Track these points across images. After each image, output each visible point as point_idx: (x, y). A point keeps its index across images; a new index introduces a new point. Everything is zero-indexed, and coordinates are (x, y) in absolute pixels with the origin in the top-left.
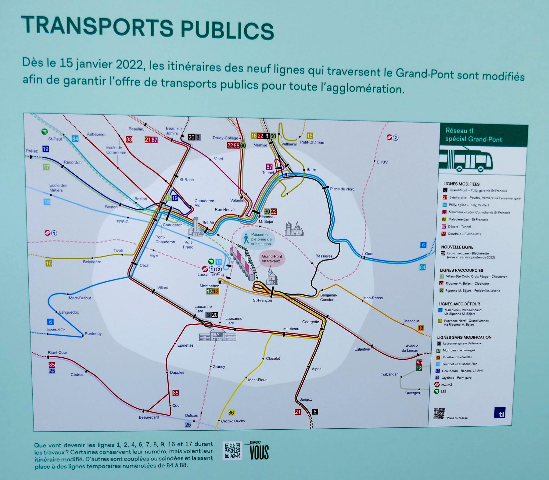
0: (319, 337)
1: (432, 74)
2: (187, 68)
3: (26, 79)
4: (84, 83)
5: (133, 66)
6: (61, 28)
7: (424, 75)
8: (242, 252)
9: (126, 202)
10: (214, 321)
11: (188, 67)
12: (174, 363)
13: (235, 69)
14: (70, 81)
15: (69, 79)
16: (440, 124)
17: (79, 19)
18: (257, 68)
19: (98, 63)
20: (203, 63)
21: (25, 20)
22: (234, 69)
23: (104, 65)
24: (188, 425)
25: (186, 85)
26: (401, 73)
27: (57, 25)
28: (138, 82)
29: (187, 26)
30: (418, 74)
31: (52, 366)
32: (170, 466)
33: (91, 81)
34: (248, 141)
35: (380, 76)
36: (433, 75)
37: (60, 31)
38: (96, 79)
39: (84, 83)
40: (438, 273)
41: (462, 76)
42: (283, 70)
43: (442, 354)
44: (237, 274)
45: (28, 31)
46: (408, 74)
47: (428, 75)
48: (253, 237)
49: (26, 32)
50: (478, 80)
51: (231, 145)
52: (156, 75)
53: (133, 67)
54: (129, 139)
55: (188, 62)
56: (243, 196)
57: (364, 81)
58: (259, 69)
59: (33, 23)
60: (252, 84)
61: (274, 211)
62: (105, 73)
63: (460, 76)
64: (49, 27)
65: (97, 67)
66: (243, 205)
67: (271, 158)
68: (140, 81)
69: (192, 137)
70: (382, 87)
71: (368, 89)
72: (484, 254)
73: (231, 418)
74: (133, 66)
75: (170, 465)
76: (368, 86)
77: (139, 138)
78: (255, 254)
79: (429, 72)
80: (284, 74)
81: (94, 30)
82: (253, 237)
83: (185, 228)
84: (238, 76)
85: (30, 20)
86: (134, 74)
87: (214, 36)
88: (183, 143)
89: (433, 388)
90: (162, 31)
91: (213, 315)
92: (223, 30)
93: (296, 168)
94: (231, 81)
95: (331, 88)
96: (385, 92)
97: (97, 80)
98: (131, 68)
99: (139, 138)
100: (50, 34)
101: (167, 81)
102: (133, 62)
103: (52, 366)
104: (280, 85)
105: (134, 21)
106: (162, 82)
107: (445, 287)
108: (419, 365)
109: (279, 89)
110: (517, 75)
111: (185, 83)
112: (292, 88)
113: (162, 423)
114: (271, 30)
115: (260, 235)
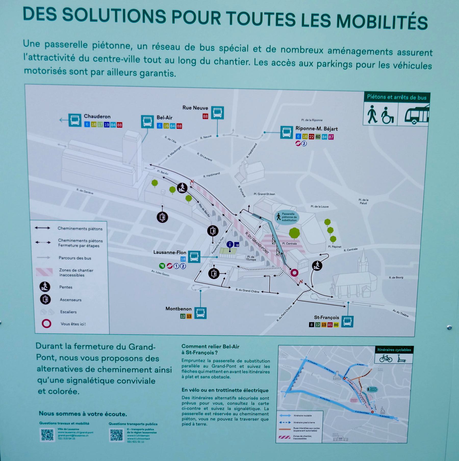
2: (273, 51)
3: (30, 57)
4: (46, 59)
6: (168, 118)
13: (256, 49)
16: (364, 92)
17: (152, 11)
20: (99, 42)
21: (229, 15)
29: (177, 14)
33: (232, 62)
37: (168, 119)
38: (236, 60)
39: (30, 59)
41: (73, 72)
48: (283, 215)
49: (23, 19)
50: (432, 56)
58: (313, 50)
60: (280, 62)
70: (32, 55)
72: (291, 214)
80: (359, 55)
81: (71, 18)
82: (283, 215)
85: (271, 16)
87: (369, 27)
90: (48, 16)
92: (376, 22)
96: (237, 65)
97: (146, 59)
101: (113, 58)
104: (371, 64)
105: (369, 17)
106: (144, 59)
109: (369, 67)
110: (158, 44)
114: (426, 22)
115: (288, 214)
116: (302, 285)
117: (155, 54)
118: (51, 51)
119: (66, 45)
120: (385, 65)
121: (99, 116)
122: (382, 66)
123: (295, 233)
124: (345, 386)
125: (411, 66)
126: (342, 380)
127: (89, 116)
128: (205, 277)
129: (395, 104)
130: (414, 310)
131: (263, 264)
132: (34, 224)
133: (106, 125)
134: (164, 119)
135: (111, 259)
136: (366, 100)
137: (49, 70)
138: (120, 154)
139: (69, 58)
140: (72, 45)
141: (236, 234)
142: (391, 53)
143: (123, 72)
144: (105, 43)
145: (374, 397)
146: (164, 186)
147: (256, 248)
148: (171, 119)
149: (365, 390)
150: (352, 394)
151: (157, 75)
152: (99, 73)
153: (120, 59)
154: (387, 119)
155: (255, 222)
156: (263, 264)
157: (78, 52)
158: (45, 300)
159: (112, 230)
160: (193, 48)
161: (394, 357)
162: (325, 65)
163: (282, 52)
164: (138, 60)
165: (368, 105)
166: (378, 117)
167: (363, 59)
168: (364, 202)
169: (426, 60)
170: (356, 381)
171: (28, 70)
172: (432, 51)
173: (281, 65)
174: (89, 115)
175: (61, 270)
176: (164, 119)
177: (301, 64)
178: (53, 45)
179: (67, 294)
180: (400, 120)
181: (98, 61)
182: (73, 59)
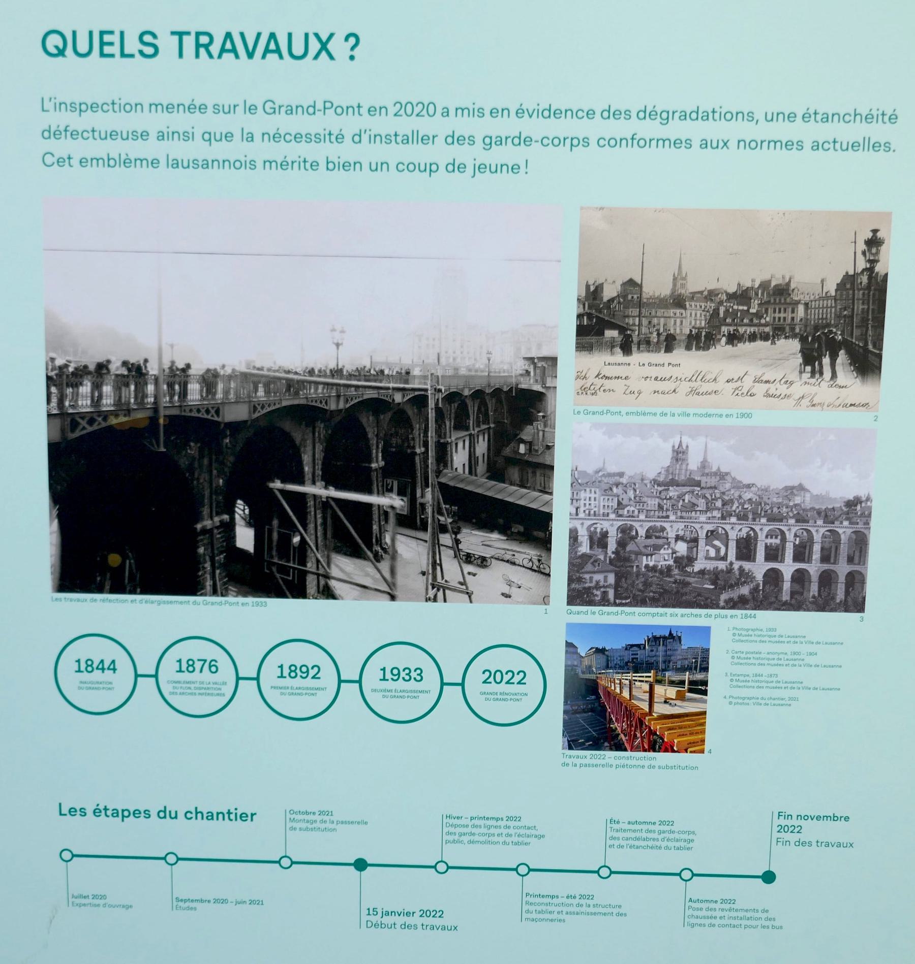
1: (325, 108)
5: (398, 112)
7: (311, 110)
14: (494, 140)
15: (491, 138)
18: (618, 113)
19: (534, 110)
21: (176, 38)
22: (616, 115)
25: (318, 140)
26: (271, 108)
27: (229, 46)
28: (529, 139)
30: (836, 117)
32: (97, 668)
35: (361, 115)
36: (326, 110)
37: (276, 56)
42: (664, 115)
45: (181, 55)
46: (283, 109)
47: (320, 110)
53: (398, 114)
55: (519, 105)
59: (189, 42)
60: (605, 140)
64: (215, 49)
65: (533, 116)
68: (149, 132)
74: (398, 112)
75: (95, 666)
76: (276, 132)
79: (320, 106)
85: (185, 38)
95: (818, 146)
98: (417, 115)
100: (216, 61)
102: (420, 106)
111: (186, 134)
112: (332, 140)
120: (302, 137)
127: (197, 813)
137: (295, 161)
139: (332, 136)
142: (628, 115)
143: (87, 160)
144: (812, 111)
151: (208, 167)
153: (531, 140)
163: (456, 116)
169: (878, 132)
171: (141, 161)
172: (361, 105)
173: (551, 145)
177: (704, 144)
181: (293, 140)
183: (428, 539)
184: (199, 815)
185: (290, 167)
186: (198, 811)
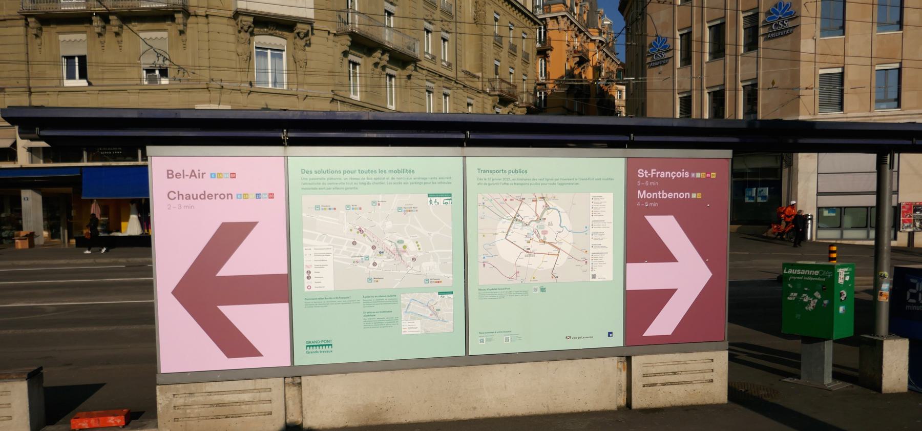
0: (558, 255)
6: (195, 176)
8: (536, 231)
9: (505, 217)
10: (529, 251)
11: (522, 180)
12: (518, 264)
23: (499, 180)
24: (522, 282)
31: (484, 265)
34: (538, 199)
37: (194, 177)
40: (591, 222)
43: (593, 259)
44: (535, 237)
47: (186, 176)
51: (533, 201)
52: (513, 182)
54: (506, 200)
56: (537, 215)
57: (569, 182)
61: (545, 219)
62: (500, 182)
63: (596, 180)
66: (537, 217)
67: (544, 204)
69: (523, 199)
71: (570, 184)
73: (534, 279)
77: (508, 199)
78: (540, 232)
83: (521, 224)
84: (535, 182)
86: (507, 182)
88: (520, 201)
89: (591, 269)
91: (529, 249)
93: (551, 207)
94: (533, 183)
99: (508, 199)
103: (484, 265)
107: (593, 226)
108: (586, 262)
113: (514, 282)
116: (409, 267)
117: (351, 181)
118: (311, 181)
119: (317, 179)
121: (204, 195)
122: (433, 183)
123: (405, 247)
124: (428, 309)
125: (444, 183)
126: (426, 307)
127: (179, 195)
128: (371, 266)
129: (439, 198)
130: (452, 275)
131: (393, 259)
132: (304, 248)
133: (330, 209)
134: (185, 177)
135: (335, 260)
136: (429, 196)
138: (338, 220)
140: (218, 196)
141: (383, 249)
145: (439, 314)
146: (355, 231)
147: (390, 253)
148: (203, 177)
149: (435, 310)
150: (430, 312)
152: (330, 189)
154: (436, 203)
155: (389, 244)
156: (393, 259)
157: (321, 181)
158: (309, 278)
159: (335, 249)
160: (364, 179)
161: (446, 296)
162: (413, 183)
164: (344, 184)
165: (429, 198)
166: (433, 203)
167: (427, 181)
168: (430, 234)
170: (432, 307)
174: (178, 192)
175: (315, 265)
176: (184, 178)
178: (312, 179)
179: (317, 275)
180: (441, 203)
182: (320, 184)
183: (480, 107)
184: (181, 197)
185: (214, 197)
186: (180, 193)
